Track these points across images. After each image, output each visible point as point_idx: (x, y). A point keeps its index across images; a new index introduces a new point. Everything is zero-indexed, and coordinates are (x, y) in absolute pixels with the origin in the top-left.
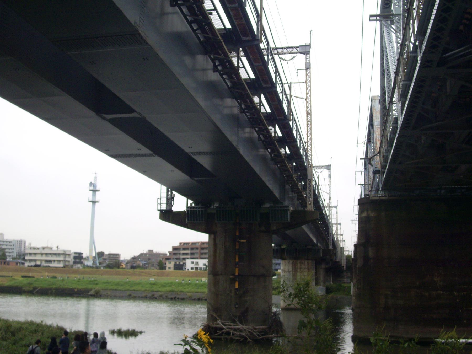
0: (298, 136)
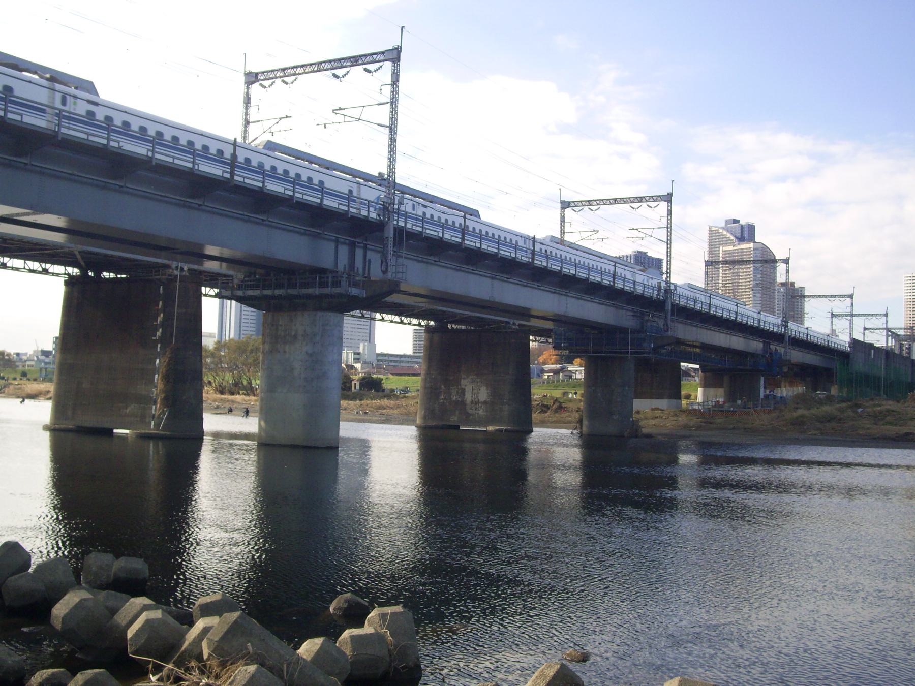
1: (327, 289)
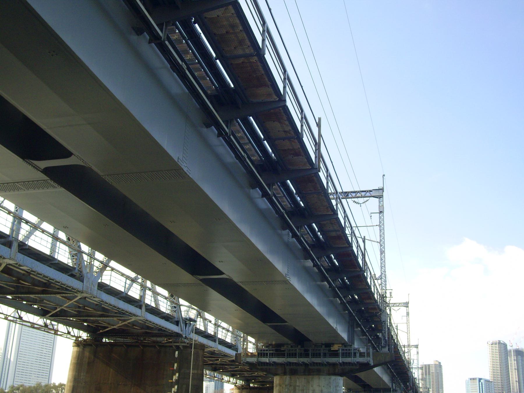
0: (372, 282)
1: (350, 358)
